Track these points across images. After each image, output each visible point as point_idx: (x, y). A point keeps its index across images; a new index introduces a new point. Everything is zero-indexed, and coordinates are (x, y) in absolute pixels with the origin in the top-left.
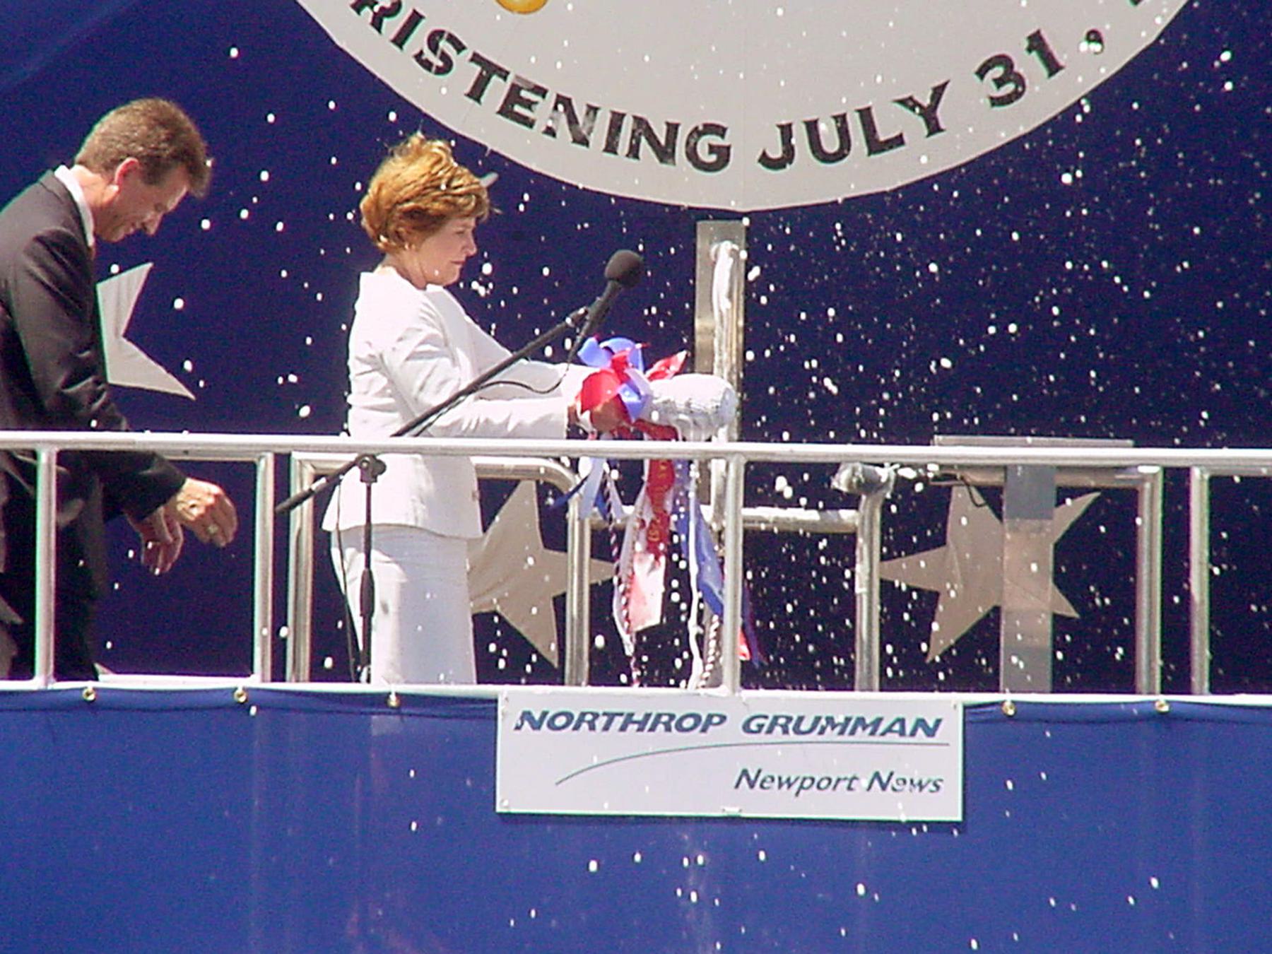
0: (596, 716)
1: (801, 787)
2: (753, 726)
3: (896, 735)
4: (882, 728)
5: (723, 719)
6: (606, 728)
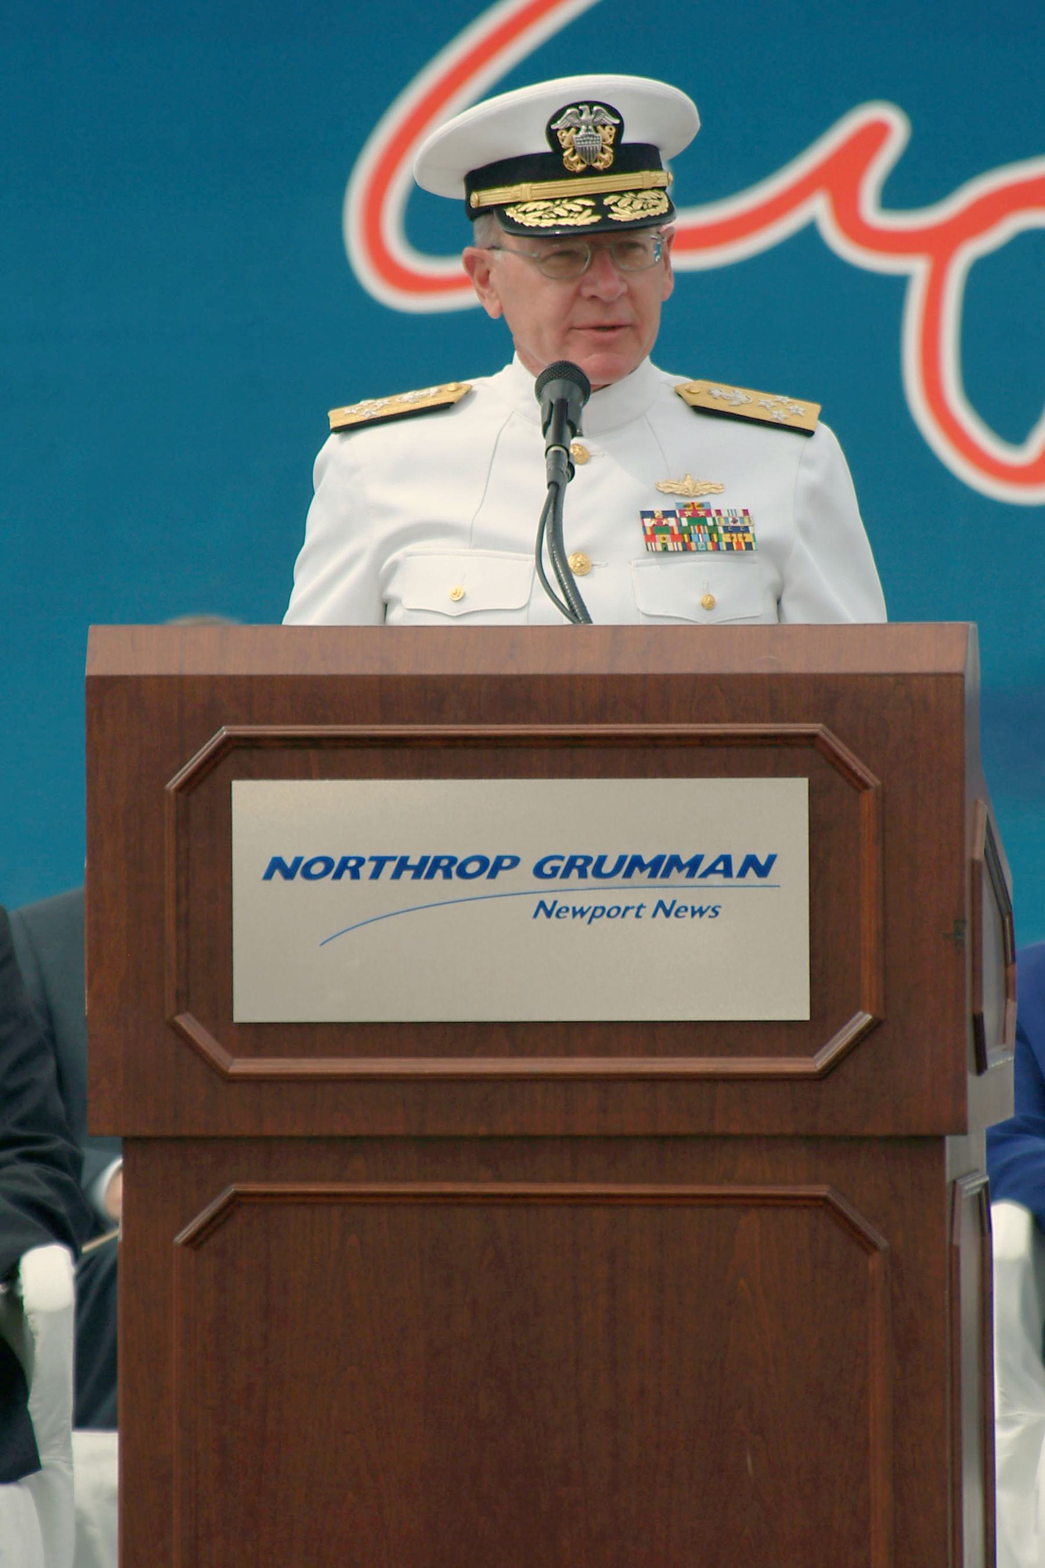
0: (361, 861)
1: (593, 916)
2: (547, 869)
3: (721, 876)
4: (701, 870)
5: (515, 861)
6: (376, 875)
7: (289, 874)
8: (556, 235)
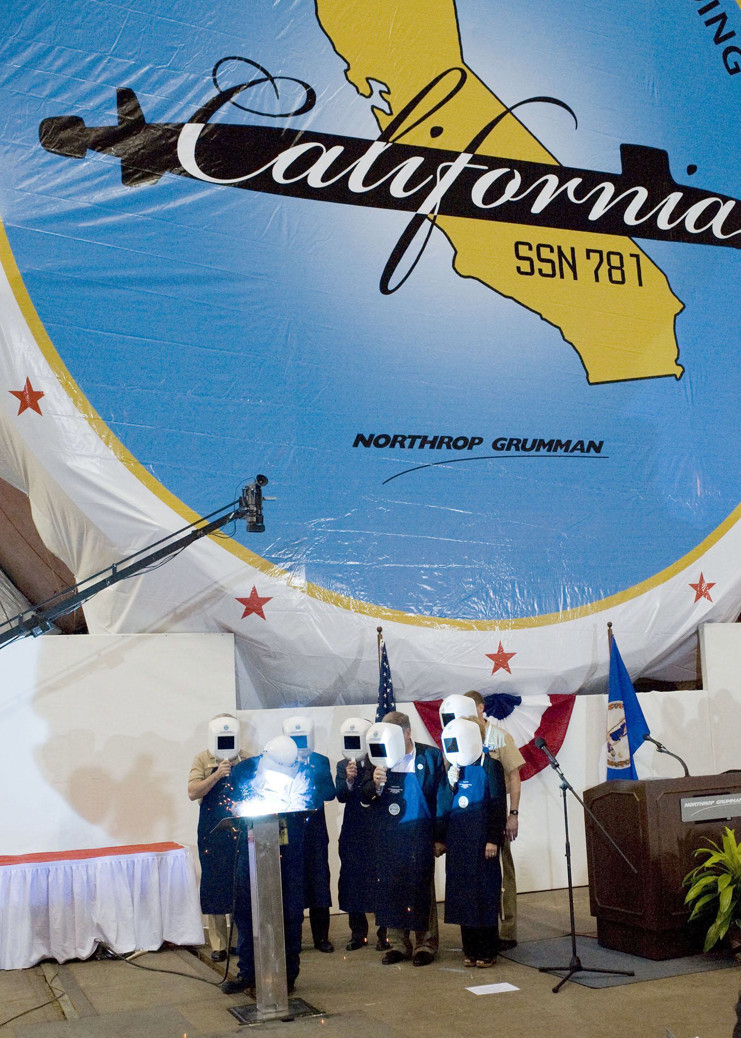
2: (499, 445)
6: (411, 446)
7: (367, 444)
8: (226, 924)
